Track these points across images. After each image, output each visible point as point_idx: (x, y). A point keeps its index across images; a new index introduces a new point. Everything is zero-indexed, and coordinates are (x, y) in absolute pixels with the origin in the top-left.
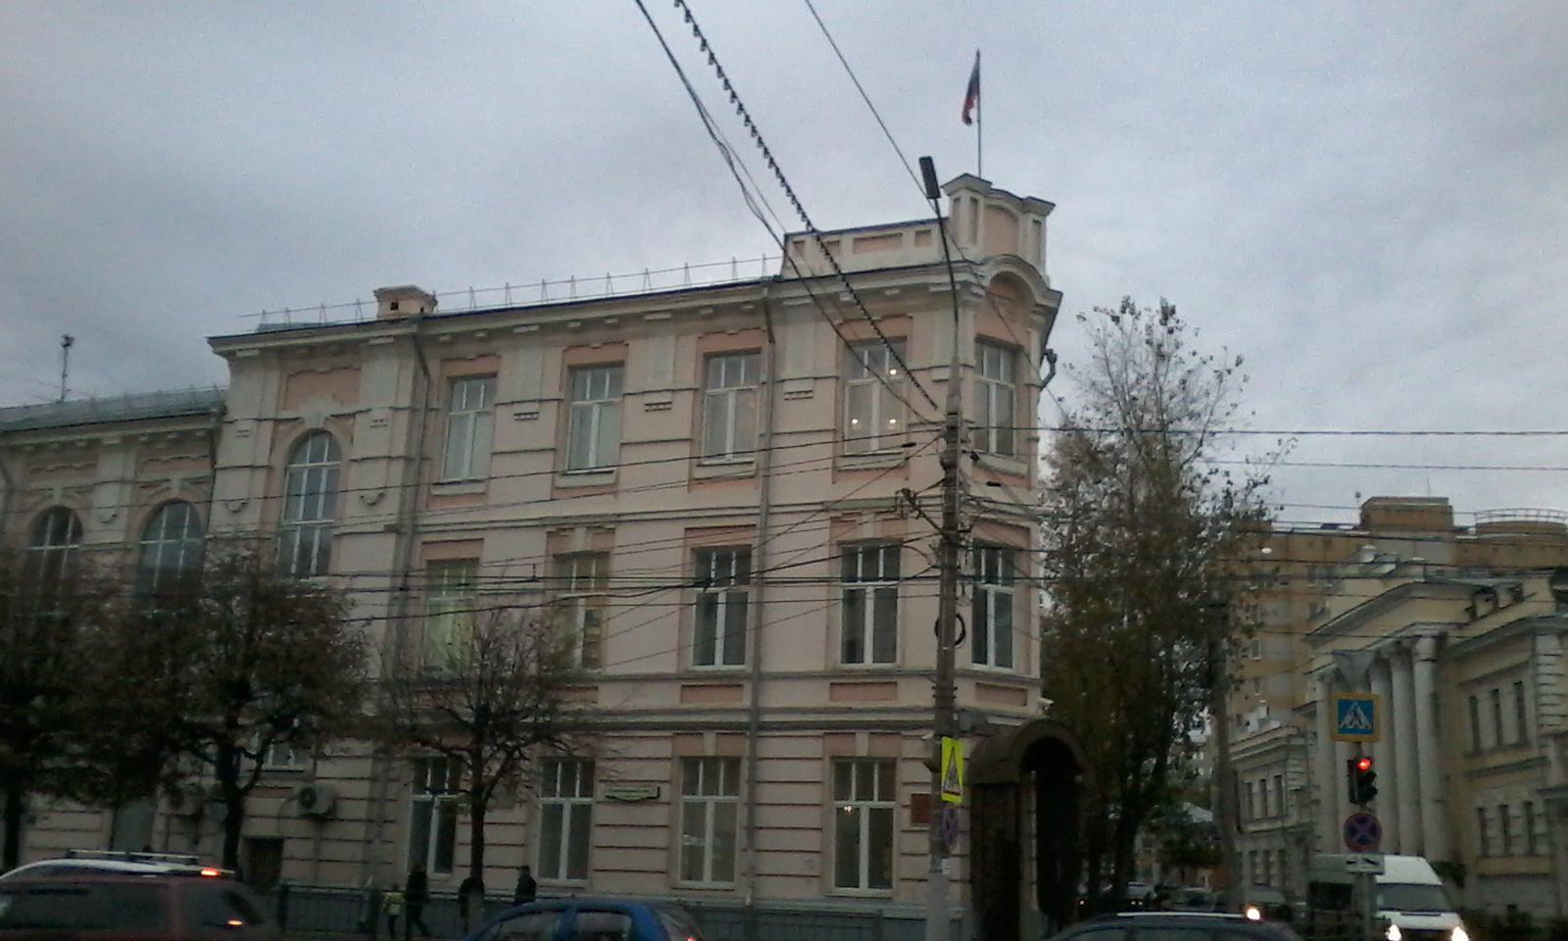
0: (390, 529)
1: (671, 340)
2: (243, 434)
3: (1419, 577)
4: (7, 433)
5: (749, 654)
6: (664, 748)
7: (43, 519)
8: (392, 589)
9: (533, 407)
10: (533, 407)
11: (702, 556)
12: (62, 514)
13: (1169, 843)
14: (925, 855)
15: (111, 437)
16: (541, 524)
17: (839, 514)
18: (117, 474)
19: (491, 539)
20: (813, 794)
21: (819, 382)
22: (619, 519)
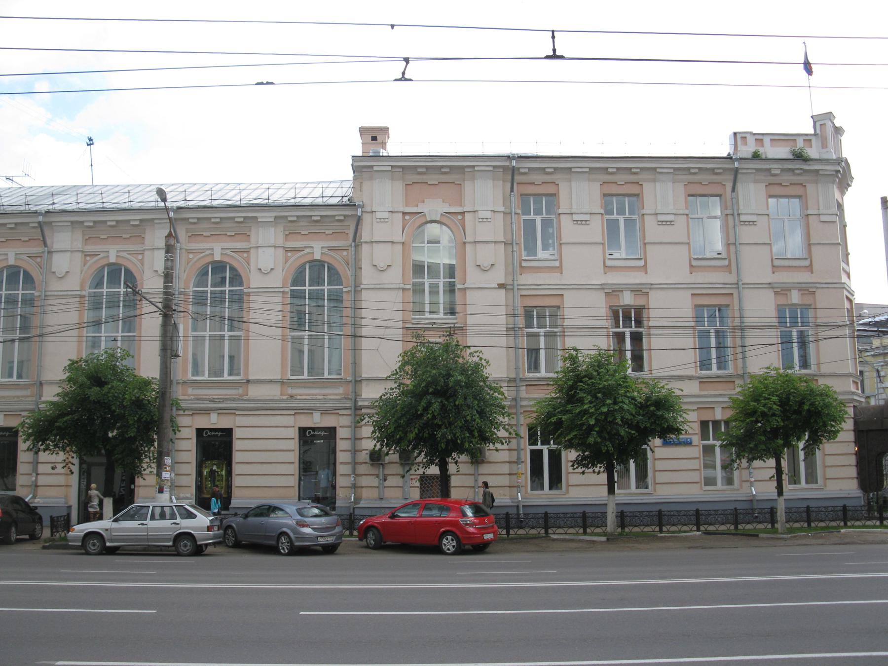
0: (501, 286)
1: (670, 184)
2: (383, 221)
3: (398, 321)
4: (6, 214)
5: (646, 368)
6: (290, 420)
7: (301, 271)
8: (80, 326)
9: (587, 217)
10: (587, 217)
11: (698, 308)
12: (219, 267)
13: (579, 463)
14: (349, 475)
15: (268, 216)
16: (602, 287)
17: (779, 290)
18: (272, 242)
19: (653, 294)
20: (695, 464)
21: (593, 216)
22: (651, 286)
